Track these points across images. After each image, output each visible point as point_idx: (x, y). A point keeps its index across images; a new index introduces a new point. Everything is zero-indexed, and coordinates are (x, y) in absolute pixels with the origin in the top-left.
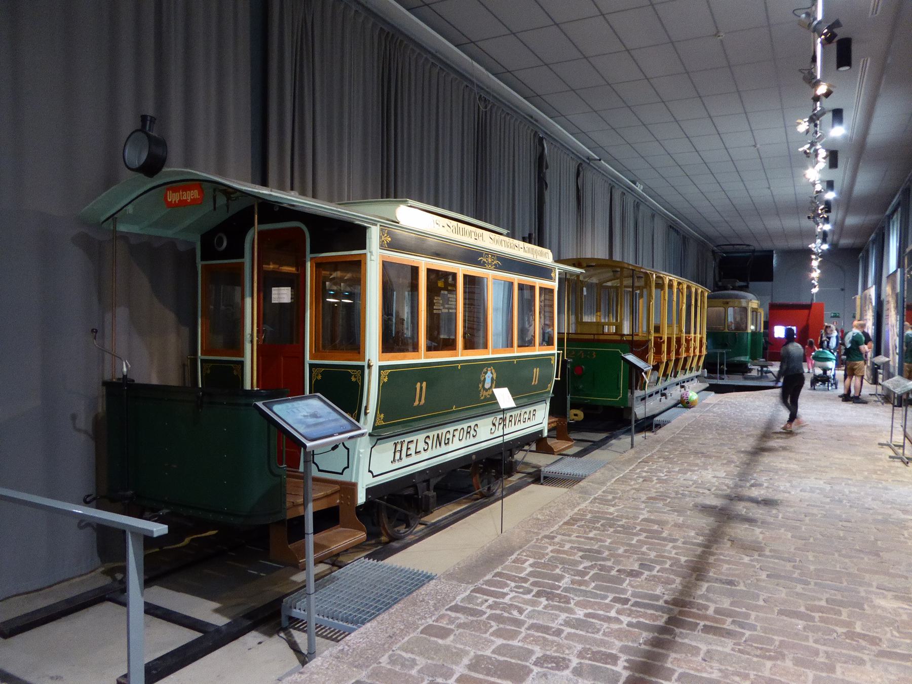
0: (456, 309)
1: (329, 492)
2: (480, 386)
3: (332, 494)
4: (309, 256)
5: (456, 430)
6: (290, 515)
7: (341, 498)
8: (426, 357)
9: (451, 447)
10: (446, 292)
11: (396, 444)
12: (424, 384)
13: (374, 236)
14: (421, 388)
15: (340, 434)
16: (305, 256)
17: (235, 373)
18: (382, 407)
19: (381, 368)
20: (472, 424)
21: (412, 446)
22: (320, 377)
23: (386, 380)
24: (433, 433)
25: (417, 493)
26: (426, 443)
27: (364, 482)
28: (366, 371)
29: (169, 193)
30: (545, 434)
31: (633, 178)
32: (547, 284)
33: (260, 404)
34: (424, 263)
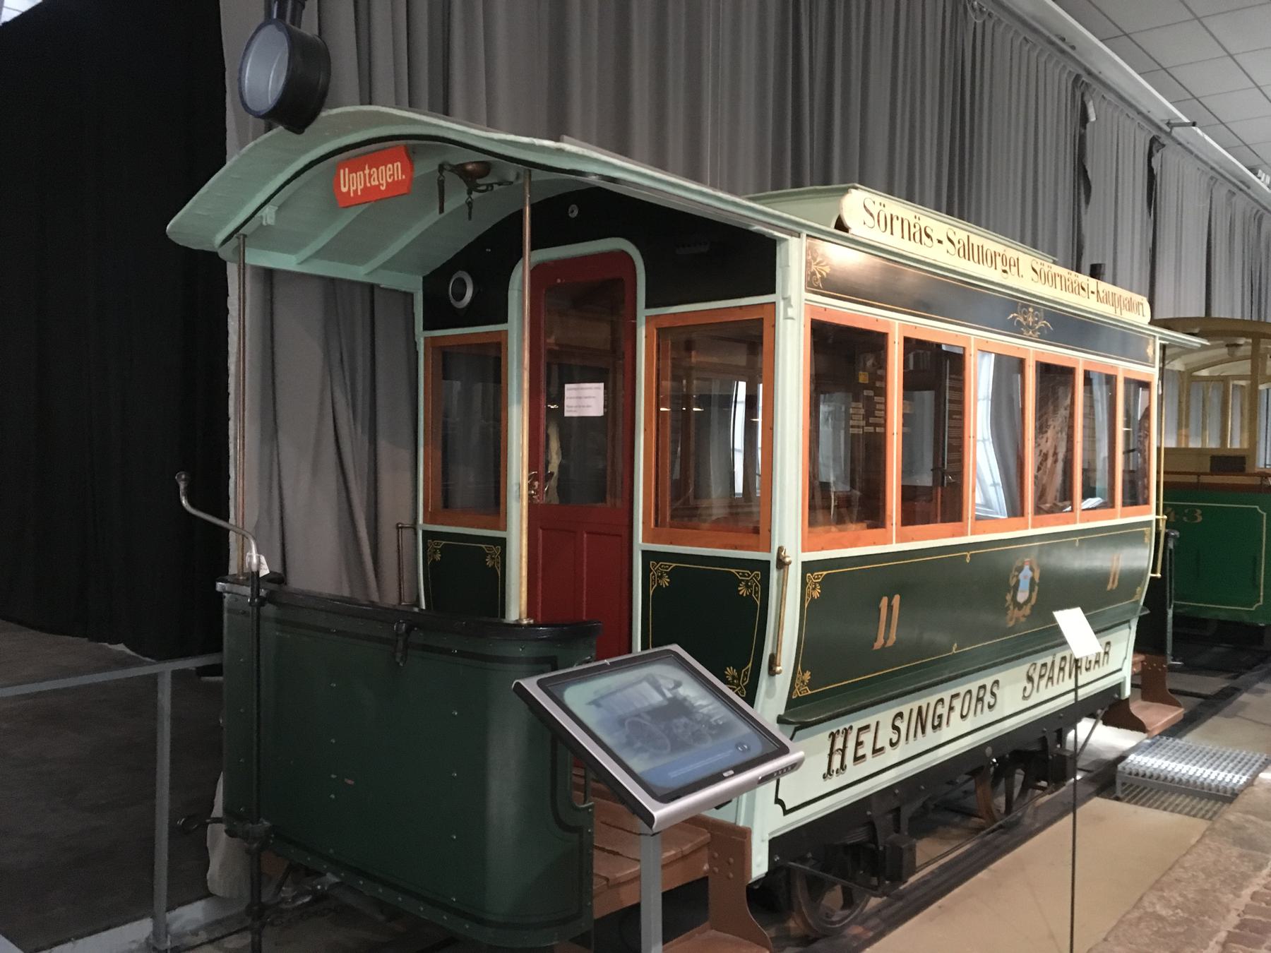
0: (884, 425)
1: (687, 848)
2: (1009, 597)
3: (694, 852)
4: (643, 313)
5: (957, 695)
6: (602, 907)
7: (712, 859)
8: (901, 539)
9: (946, 733)
10: (871, 393)
11: (833, 736)
12: (897, 599)
13: (794, 260)
14: (890, 607)
15: (739, 769)
16: (635, 317)
17: (489, 563)
18: (808, 654)
19: (808, 567)
20: (988, 682)
21: (867, 738)
22: (665, 582)
23: (816, 594)
24: (909, 706)
25: (874, 838)
26: (895, 728)
27: (765, 822)
28: (774, 574)
29: (344, 174)
30: (1127, 692)
31: (1255, 161)
32: (1124, 368)
33: (530, 684)
34: (898, 326)
